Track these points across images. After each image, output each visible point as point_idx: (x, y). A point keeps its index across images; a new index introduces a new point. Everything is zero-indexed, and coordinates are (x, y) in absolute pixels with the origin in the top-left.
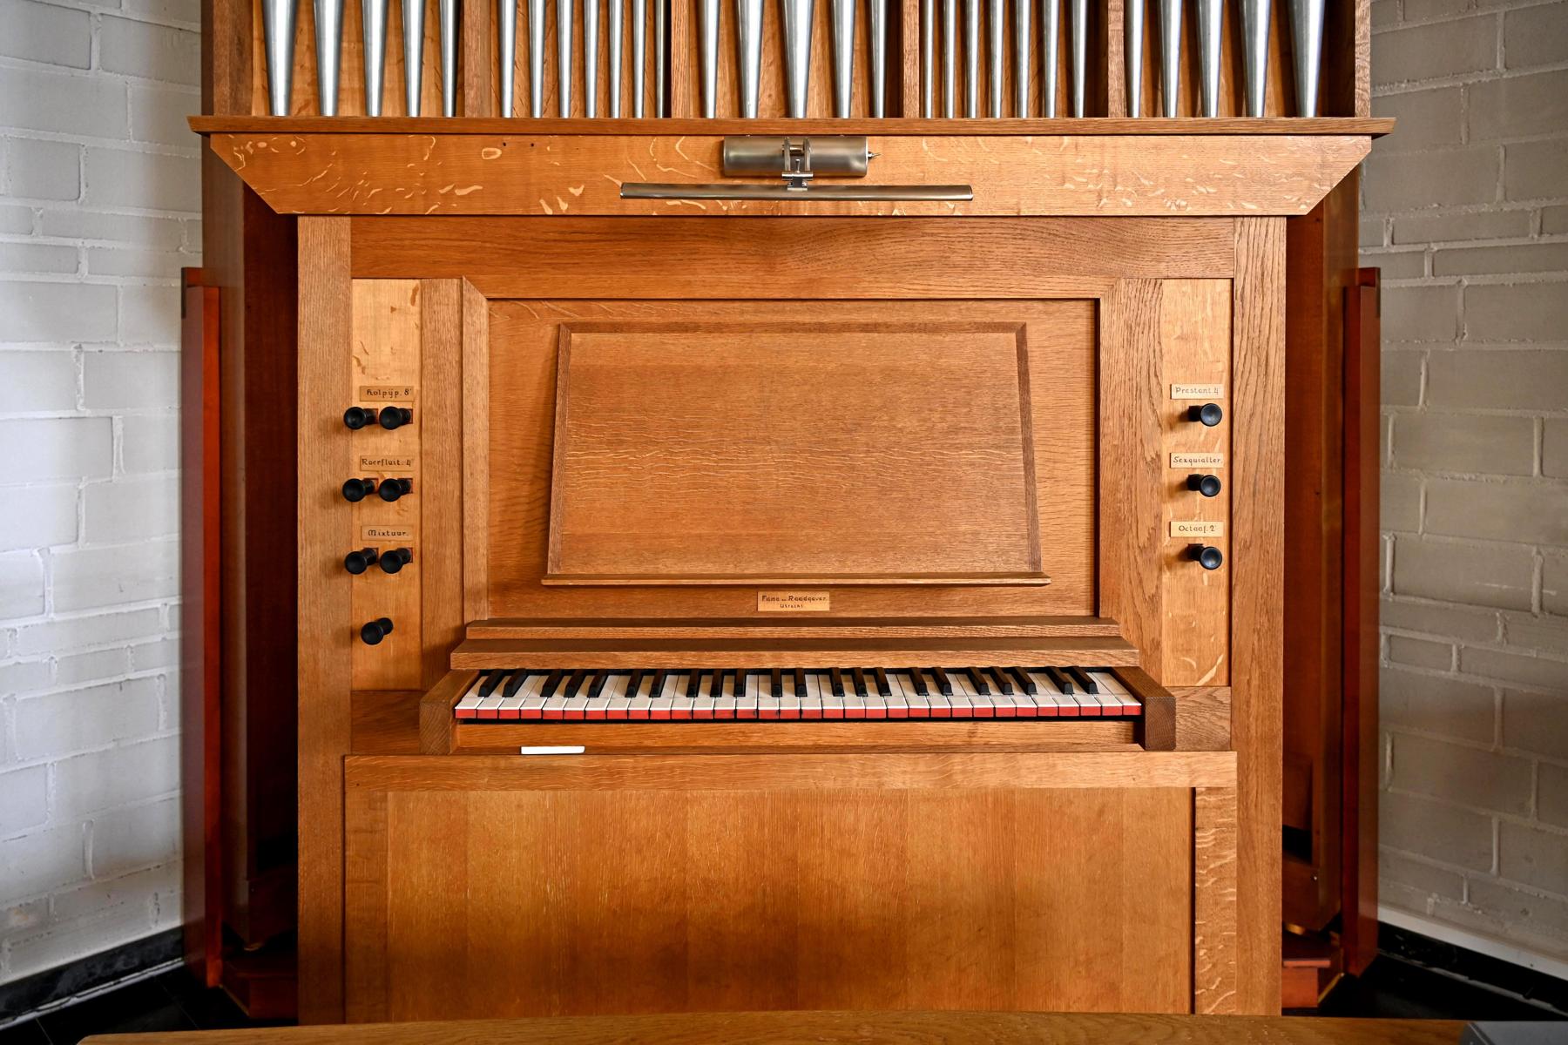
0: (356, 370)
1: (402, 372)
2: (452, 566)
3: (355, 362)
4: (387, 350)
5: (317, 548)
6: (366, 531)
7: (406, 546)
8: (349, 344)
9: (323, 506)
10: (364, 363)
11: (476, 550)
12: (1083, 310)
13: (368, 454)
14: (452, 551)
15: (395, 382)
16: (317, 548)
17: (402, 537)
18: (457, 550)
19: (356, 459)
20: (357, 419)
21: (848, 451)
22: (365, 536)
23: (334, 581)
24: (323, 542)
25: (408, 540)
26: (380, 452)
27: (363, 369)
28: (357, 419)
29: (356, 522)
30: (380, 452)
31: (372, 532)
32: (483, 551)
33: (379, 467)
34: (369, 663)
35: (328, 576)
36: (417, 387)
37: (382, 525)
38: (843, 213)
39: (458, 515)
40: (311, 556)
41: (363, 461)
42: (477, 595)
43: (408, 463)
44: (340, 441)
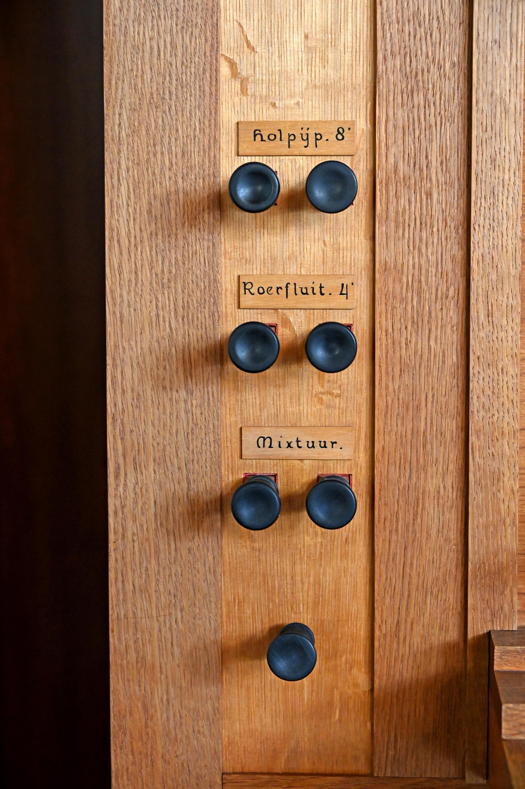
0: (228, 88)
1: (330, 90)
2: (439, 517)
3: (225, 70)
4: (296, 41)
5: (150, 474)
6: (250, 437)
7: (340, 470)
8: (216, 26)
9: (162, 385)
10: (244, 70)
11: (497, 478)
12: (242, 305)
13: (254, 272)
14: (440, 481)
15: (312, 111)
16: (150, 474)
17: (329, 453)
18: (452, 479)
19: (228, 283)
20: (257, 192)
21: (494, 525)
22: (250, 449)
23: (185, 545)
24: (161, 461)
25: (346, 458)
26: (302, 266)
27: (244, 82)
28: (257, 192)
29: (231, 420)
30: (302, 266)
31: (265, 441)
32: (510, 482)
33: (279, 301)
34: (259, 711)
35: (173, 534)
36: (362, 125)
37: (303, 425)
38: (249, 157)
39: (454, 402)
40: (134, 495)
41: (243, 286)
42: (496, 576)
43: (344, 291)
44: (198, 242)
